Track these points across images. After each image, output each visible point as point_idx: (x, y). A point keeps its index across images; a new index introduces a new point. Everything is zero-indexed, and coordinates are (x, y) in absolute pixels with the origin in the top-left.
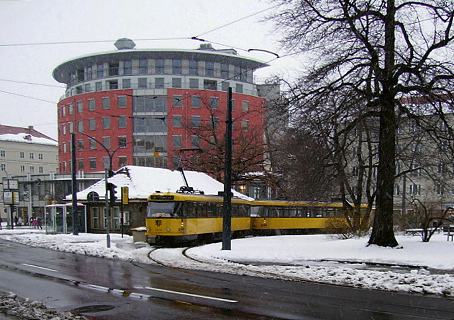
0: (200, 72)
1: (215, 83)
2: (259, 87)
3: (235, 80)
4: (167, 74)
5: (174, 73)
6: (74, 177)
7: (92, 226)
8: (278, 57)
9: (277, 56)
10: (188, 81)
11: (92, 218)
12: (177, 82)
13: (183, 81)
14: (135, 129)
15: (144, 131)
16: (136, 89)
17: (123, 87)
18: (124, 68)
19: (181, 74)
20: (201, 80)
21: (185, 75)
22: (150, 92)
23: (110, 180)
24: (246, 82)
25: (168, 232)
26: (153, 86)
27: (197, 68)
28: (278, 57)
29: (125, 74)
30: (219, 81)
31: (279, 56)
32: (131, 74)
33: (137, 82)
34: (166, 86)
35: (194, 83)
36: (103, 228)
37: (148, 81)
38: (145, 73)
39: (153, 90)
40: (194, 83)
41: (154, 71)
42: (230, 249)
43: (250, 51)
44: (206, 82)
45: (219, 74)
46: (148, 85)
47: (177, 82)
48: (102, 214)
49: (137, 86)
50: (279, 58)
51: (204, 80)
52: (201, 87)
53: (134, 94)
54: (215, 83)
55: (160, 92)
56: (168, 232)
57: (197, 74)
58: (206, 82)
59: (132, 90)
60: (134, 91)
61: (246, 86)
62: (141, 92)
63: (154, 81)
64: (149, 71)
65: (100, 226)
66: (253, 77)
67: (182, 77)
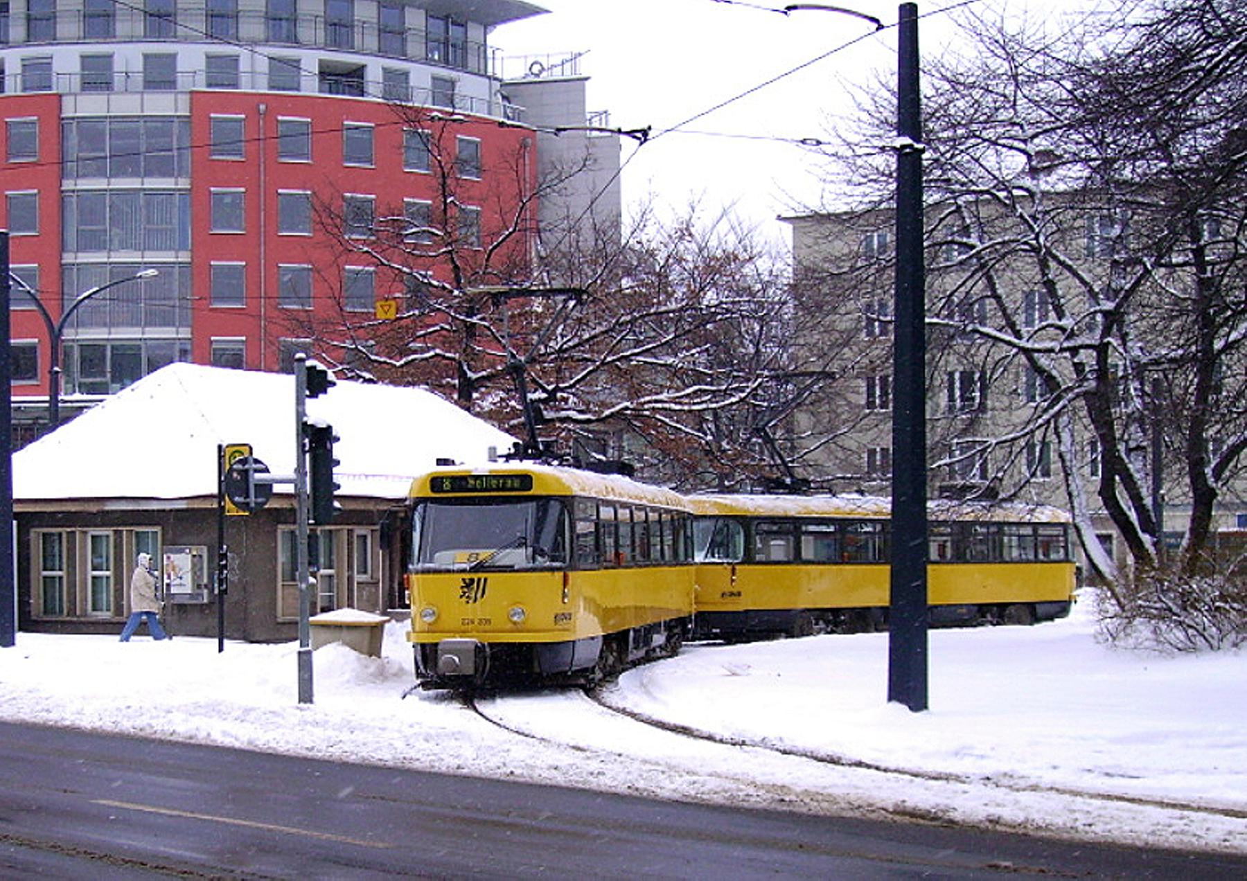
0: (304, 33)
1: (358, 72)
2: (509, 91)
3: (427, 61)
4: (186, 40)
5: (211, 36)
6: (54, 400)
7: (36, 602)
8: (880, 27)
9: (875, 26)
10: (263, 65)
11: (38, 573)
12: (222, 69)
13: (244, 65)
14: (71, 237)
15: (100, 247)
16: (75, 95)
17: (25, 89)
18: (29, 19)
19: (237, 41)
20: (311, 60)
21: (254, 43)
22: (125, 104)
23: (319, 411)
24: (464, 68)
25: (517, 628)
26: (139, 79)
27: (294, 21)
28: (880, 27)
29: (29, 39)
30: (375, 68)
31: (883, 22)
32: (54, 40)
33: (76, 67)
34: (183, 82)
35: (285, 70)
36: (85, 614)
37: (118, 65)
38: (108, 35)
39: (138, 97)
40: (285, 70)
41: (140, 29)
42: (890, 699)
43: (793, 12)
44: (328, 74)
45: (372, 42)
46: (118, 80)
47: (222, 69)
48: (84, 556)
49: (76, 82)
50: (881, 32)
51: (322, 63)
52: (310, 87)
53: (68, 112)
54: (358, 72)
55: (162, 104)
56: (517, 628)
57: (295, 41)
58: (328, 74)
59: (60, 96)
60: (68, 103)
61: (470, 88)
62: (91, 105)
63: (139, 65)
64: (121, 28)
65: (72, 601)
66: (489, 52)
67: (243, 53)
